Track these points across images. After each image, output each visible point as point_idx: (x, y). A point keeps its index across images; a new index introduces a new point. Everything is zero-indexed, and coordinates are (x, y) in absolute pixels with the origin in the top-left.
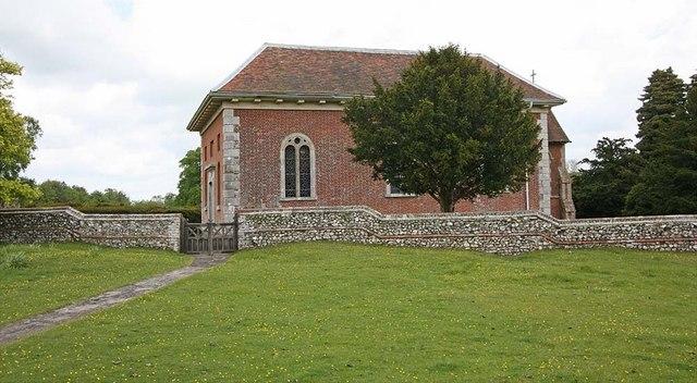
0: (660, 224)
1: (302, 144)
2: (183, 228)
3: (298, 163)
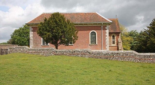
0: (73, 51)
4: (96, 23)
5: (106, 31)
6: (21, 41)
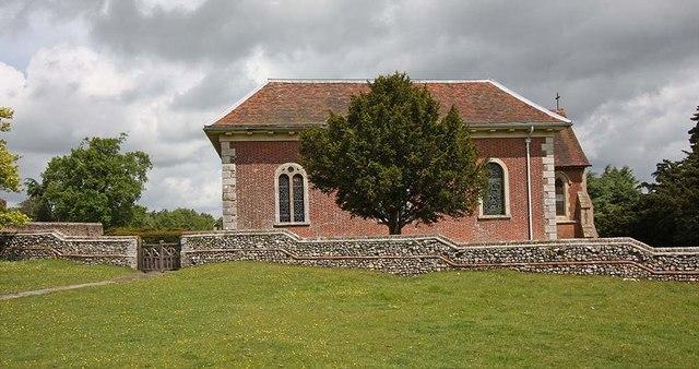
0: (553, 248)
1: (295, 172)
2: (140, 249)
3: (291, 190)
4: (509, 124)
5: (545, 160)
6: (81, 207)
